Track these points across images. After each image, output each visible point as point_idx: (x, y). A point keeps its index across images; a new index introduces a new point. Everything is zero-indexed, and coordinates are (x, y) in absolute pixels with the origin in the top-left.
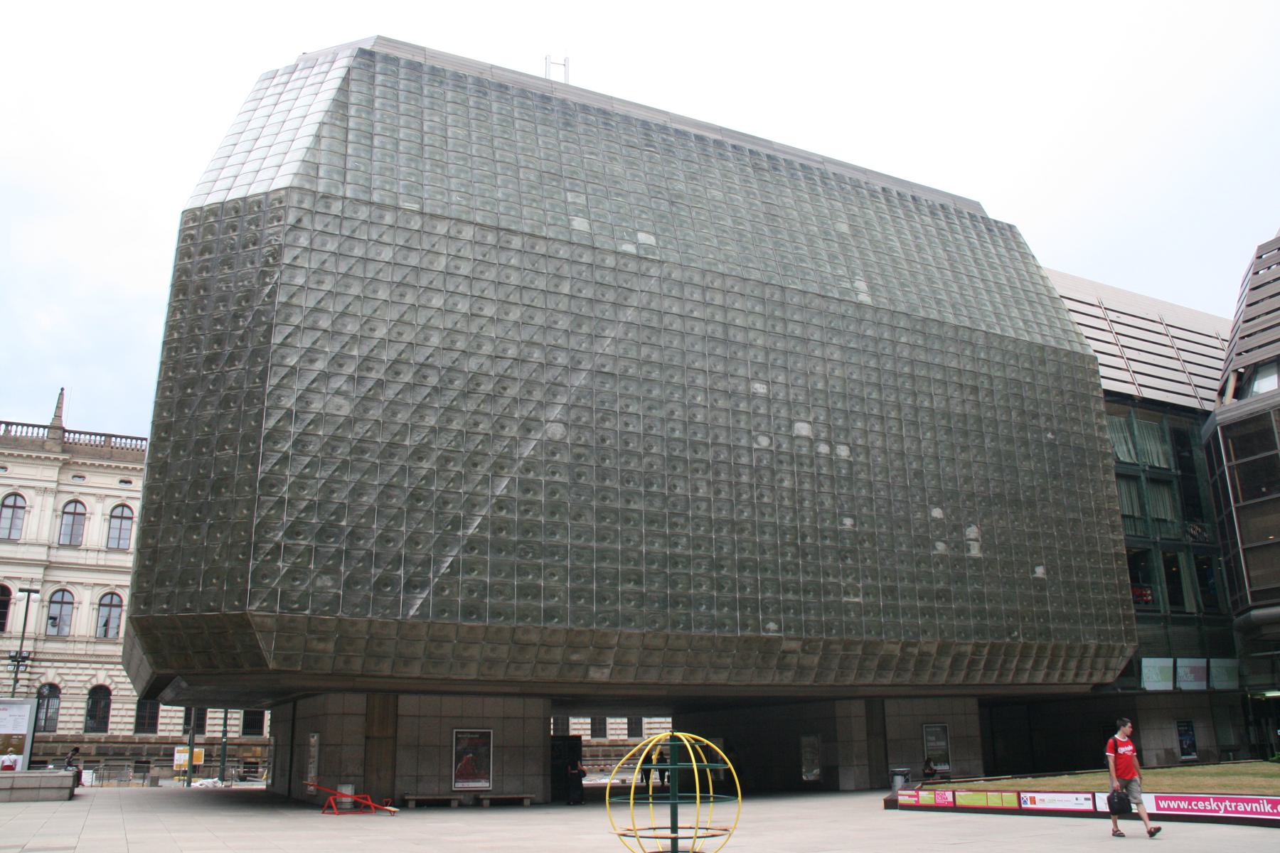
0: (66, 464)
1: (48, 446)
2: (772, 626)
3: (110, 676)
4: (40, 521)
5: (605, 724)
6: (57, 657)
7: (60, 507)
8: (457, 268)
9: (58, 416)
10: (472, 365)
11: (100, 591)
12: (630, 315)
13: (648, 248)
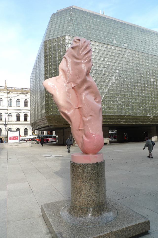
0: (8, 93)
1: (5, 90)
2: (149, 114)
3: (19, 127)
4: (5, 103)
5: (32, 127)
6: (18, 124)
7: (8, 100)
8: (96, 51)
9: (6, 85)
10: (100, 69)
11: (16, 113)
12: (124, 59)
13: (126, 46)
